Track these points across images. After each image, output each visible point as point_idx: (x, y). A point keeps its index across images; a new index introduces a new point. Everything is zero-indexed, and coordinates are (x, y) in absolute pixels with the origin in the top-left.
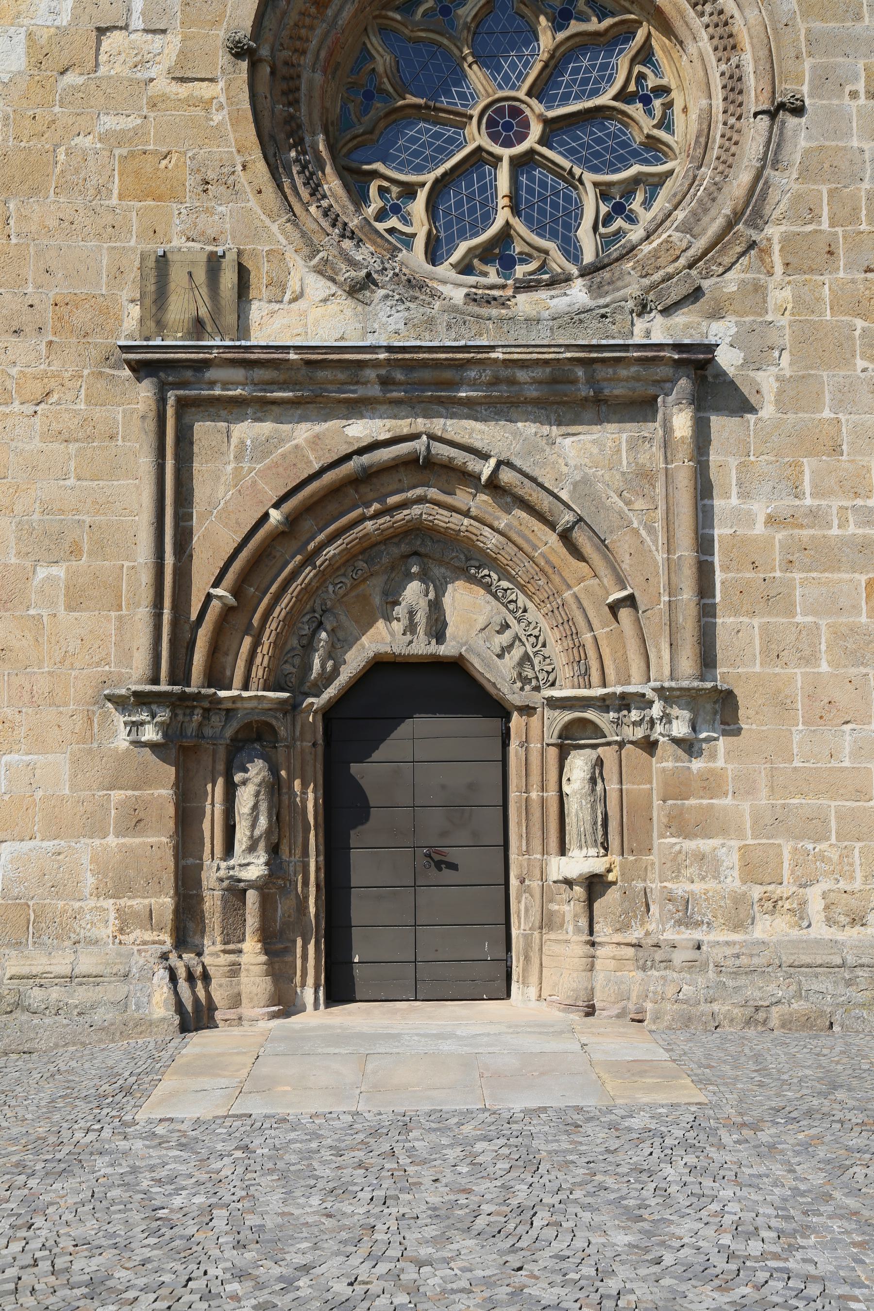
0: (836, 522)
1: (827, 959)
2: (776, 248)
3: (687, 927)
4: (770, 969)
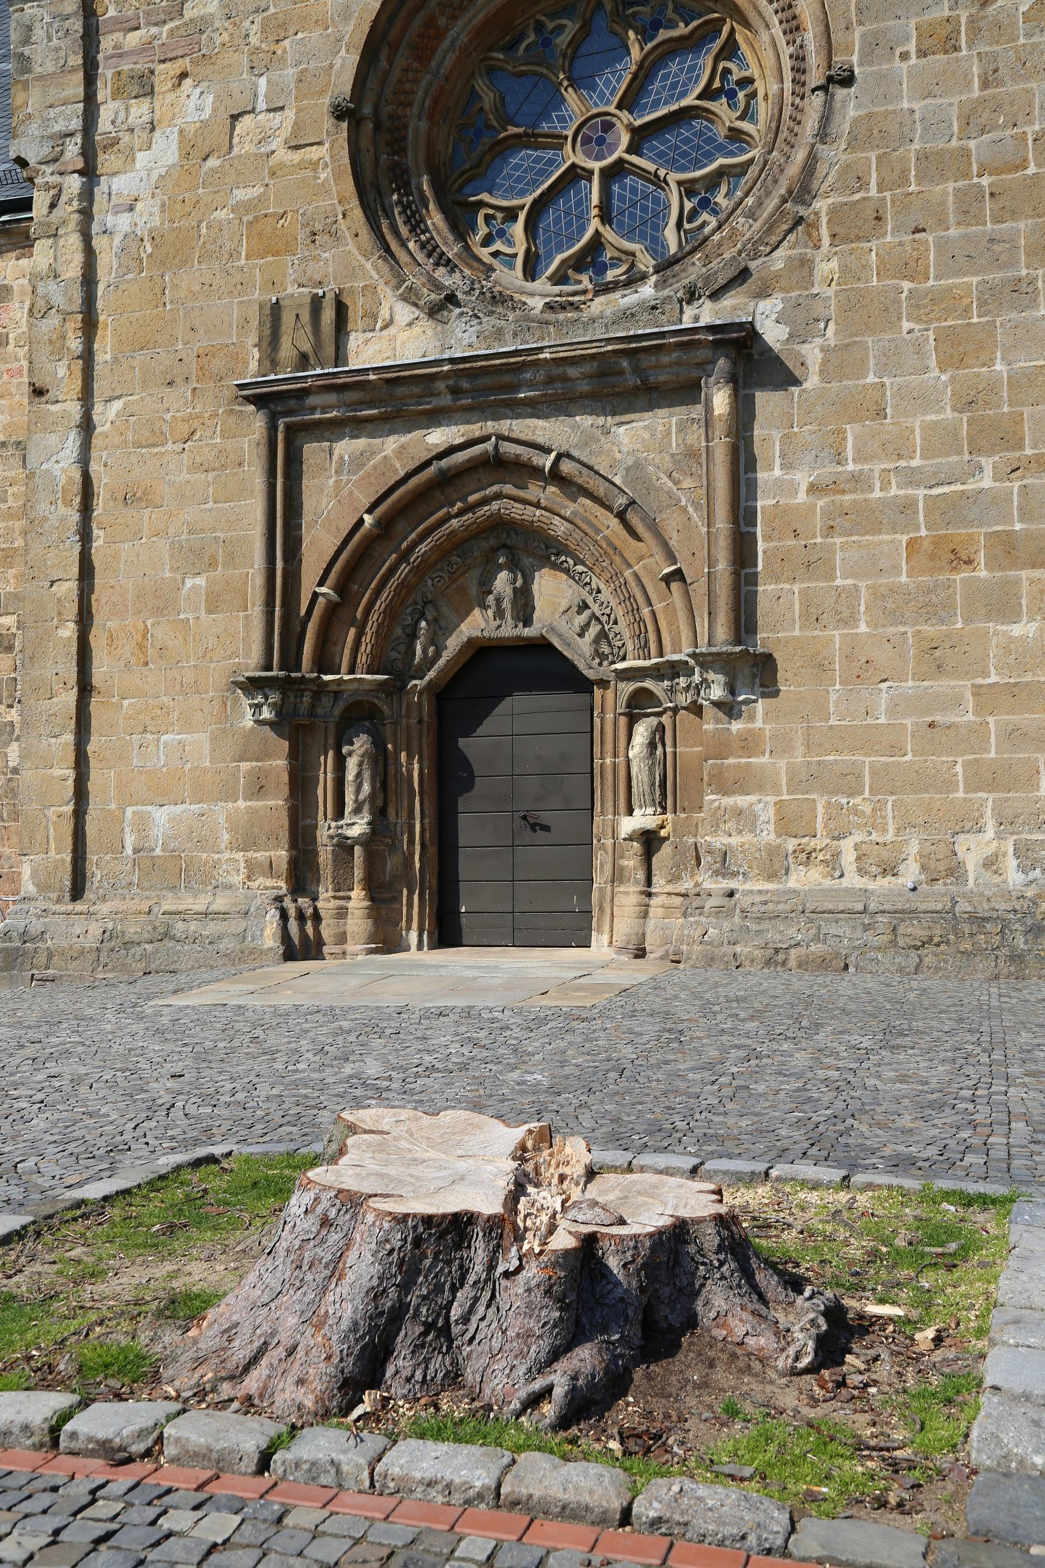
0: (878, 485)
1: (849, 905)
2: (824, 220)
3: (724, 877)
4: (793, 915)
